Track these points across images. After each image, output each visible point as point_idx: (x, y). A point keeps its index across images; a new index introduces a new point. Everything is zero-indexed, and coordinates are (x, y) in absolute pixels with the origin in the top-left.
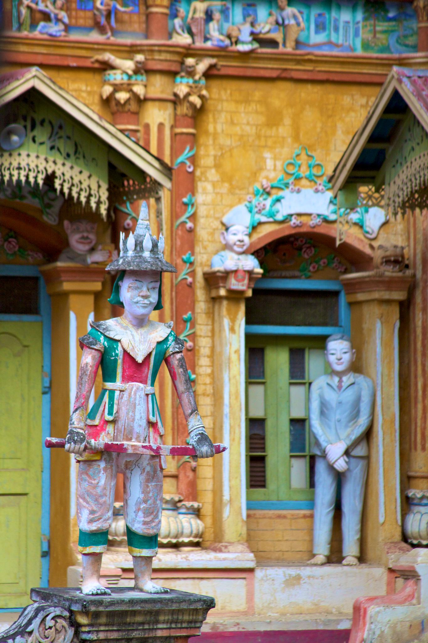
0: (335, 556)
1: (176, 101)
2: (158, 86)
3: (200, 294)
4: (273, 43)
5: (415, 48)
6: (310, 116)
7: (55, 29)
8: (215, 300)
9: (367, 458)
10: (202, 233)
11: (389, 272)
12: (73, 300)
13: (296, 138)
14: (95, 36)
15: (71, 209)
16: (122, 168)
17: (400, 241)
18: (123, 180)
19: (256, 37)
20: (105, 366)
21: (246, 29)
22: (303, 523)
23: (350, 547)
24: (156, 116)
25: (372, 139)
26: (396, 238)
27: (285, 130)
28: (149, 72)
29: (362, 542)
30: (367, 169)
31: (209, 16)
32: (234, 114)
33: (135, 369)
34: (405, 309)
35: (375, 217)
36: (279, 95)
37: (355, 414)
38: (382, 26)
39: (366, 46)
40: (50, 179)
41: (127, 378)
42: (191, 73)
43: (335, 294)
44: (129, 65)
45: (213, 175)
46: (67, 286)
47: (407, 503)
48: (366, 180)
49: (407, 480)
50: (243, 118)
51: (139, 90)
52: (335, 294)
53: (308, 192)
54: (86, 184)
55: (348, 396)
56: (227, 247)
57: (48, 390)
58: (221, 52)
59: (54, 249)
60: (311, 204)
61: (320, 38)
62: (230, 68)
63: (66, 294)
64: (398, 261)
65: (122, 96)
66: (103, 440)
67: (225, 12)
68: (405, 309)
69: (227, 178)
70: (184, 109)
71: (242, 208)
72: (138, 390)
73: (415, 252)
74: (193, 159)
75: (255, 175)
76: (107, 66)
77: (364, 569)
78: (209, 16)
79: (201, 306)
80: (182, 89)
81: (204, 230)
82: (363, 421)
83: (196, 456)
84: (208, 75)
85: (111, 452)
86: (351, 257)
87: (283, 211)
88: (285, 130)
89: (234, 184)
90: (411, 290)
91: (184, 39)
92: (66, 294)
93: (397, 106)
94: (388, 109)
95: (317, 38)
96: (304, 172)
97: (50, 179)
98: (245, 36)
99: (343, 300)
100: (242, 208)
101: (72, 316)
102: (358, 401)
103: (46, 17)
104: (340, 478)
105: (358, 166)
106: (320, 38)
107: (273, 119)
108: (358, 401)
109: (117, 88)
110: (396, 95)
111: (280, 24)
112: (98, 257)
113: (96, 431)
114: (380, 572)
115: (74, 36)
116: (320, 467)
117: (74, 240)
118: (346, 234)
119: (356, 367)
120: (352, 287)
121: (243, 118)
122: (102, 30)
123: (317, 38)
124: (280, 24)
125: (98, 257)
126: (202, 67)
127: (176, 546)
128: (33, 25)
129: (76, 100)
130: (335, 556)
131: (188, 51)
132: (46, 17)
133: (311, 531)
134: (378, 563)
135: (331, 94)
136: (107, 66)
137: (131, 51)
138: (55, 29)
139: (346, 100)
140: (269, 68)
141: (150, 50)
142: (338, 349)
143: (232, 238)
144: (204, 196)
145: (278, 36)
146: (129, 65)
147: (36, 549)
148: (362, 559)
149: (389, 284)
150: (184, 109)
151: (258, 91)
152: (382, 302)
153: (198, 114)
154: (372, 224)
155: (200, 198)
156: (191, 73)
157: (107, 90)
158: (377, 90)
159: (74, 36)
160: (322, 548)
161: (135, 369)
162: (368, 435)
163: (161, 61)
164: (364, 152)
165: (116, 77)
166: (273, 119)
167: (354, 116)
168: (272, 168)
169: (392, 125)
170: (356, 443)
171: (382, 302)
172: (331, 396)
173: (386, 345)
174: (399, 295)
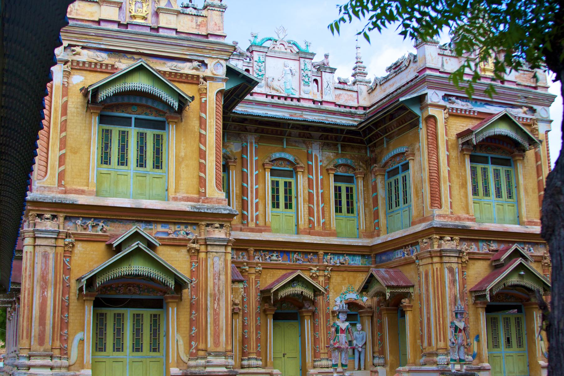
0: (359, 369)
1: (325, 276)
2: (321, 273)
3: (331, 315)
4: (344, 264)
5: (372, 264)
6: (351, 278)
7: (301, 262)
8: (334, 316)
9: (365, 348)
10: (331, 303)
11: (369, 310)
12: (306, 317)
13: (349, 283)
14: (308, 263)
15: (305, 298)
16: (316, 290)
17: (370, 303)
18: (316, 291)
19: (340, 263)
20: (337, 331)
21: (338, 261)
22: (352, 362)
23: (362, 367)
24: (321, 279)
25: (366, 283)
26: (369, 303)
27: (346, 281)
28: (319, 270)
29: (365, 366)
30: (365, 289)
31: (331, 259)
32: (336, 278)
33: (343, 331)
34: (372, 317)
35: (365, 299)
36: (345, 274)
37: (363, 339)
38: (365, 260)
39: (362, 264)
40: (302, 292)
41: (341, 333)
42: (328, 270)
43: (357, 315)
44: (316, 269)
45: (332, 291)
46: (304, 314)
47: (374, 357)
48: (364, 291)
49: (373, 352)
50: (338, 279)
51: (318, 274)
52: (357, 315)
53: (351, 294)
54: (308, 293)
55: (361, 335)
56: (336, 305)
57: (300, 336)
58: (333, 266)
59: (301, 307)
60: (352, 296)
61: (353, 263)
62: (335, 269)
63: (304, 316)
64: (370, 307)
65: (314, 275)
66: (337, 346)
67: (334, 258)
68: (372, 317)
69: (335, 291)
70: (327, 277)
71: (338, 297)
72: (343, 335)
73: (374, 305)
74: (329, 288)
75: (341, 290)
76: (311, 269)
77: (365, 371)
78: (331, 259)
79: (331, 318)
80: (326, 274)
81: (331, 302)
82: (364, 341)
83: (60, 349)
84: (331, 270)
85: (338, 348)
86: (361, 307)
87: (347, 298)
88: (346, 281)
89: (337, 293)
90: (373, 313)
91: (326, 263)
92: (304, 316)
93: (372, 276)
94: (370, 277)
95: (352, 263)
96: (351, 290)
97: (302, 292)
98: (338, 262)
99: (358, 316)
100: (338, 297)
101: (170, 309)
102: (363, 337)
103: (299, 260)
104: (360, 353)
105: (363, 288)
106: (353, 263)
107: (344, 279)
108: (363, 337)
109: (313, 274)
110: (371, 274)
111: (345, 260)
112: (311, 308)
113: (335, 344)
114: (369, 372)
115: (304, 263)
116: (356, 351)
117: (306, 305)
118: (361, 303)
119: (362, 330)
120: (360, 313)
121: (338, 279)
122: (310, 262)
123: (352, 263)
124: (345, 260)
125: (311, 308)
126: (330, 269)
127: (328, 367)
128: (296, 261)
129: (306, 276)
130: (359, 369)
131: (327, 266)
132: (299, 260)
133: (354, 363)
134: (368, 370)
135: (355, 274)
136: (311, 269)
137: (316, 266)
138: (301, 262)
139: (358, 275)
140: (343, 269)
141: (320, 266)
142: (359, 326)
143: (337, 304)
144: (331, 295)
145: (344, 262)
146: (316, 269)
147: (299, 369)
148: (365, 369)
149: (369, 312)
150: (327, 277)
151: (341, 273)
152: (367, 316)
153: (329, 278)
154: (365, 300)
155: (330, 296)
156: (328, 270)
157: (311, 274)
158: (366, 273)
159: (304, 263)
160: (357, 367)
161: (343, 331)
162: (365, 344)
163: (322, 268)
164: (365, 286)
165: (313, 271)
166: (344, 279)
167: (362, 278)
168: (344, 289)
169: (371, 280)
170: (363, 345)
171: (367, 316)
172: (358, 336)
173: (368, 325)
174: (371, 315)
